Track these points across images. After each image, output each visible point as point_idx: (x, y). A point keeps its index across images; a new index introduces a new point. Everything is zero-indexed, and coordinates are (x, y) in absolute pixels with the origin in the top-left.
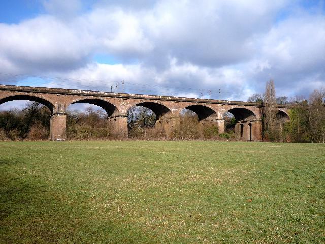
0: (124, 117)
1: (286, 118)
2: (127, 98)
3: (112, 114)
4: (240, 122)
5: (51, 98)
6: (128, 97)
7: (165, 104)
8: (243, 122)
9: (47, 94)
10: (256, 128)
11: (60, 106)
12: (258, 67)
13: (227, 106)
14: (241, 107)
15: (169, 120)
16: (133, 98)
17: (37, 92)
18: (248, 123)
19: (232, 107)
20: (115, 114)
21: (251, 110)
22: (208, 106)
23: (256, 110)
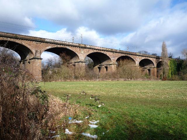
0: (82, 62)
1: (152, 65)
2: (84, 48)
3: (25, 57)
4: (98, 66)
5: (30, 45)
6: (85, 48)
7: (108, 54)
8: (100, 66)
9: (27, 42)
10: (154, 73)
11: (37, 51)
12: (87, 31)
13: (140, 57)
14: (99, 51)
15: (108, 66)
16: (88, 48)
17: (18, 39)
18: (147, 69)
19: (91, 51)
20: (28, 57)
21: (152, 60)
22: (105, 53)
23: (154, 60)
